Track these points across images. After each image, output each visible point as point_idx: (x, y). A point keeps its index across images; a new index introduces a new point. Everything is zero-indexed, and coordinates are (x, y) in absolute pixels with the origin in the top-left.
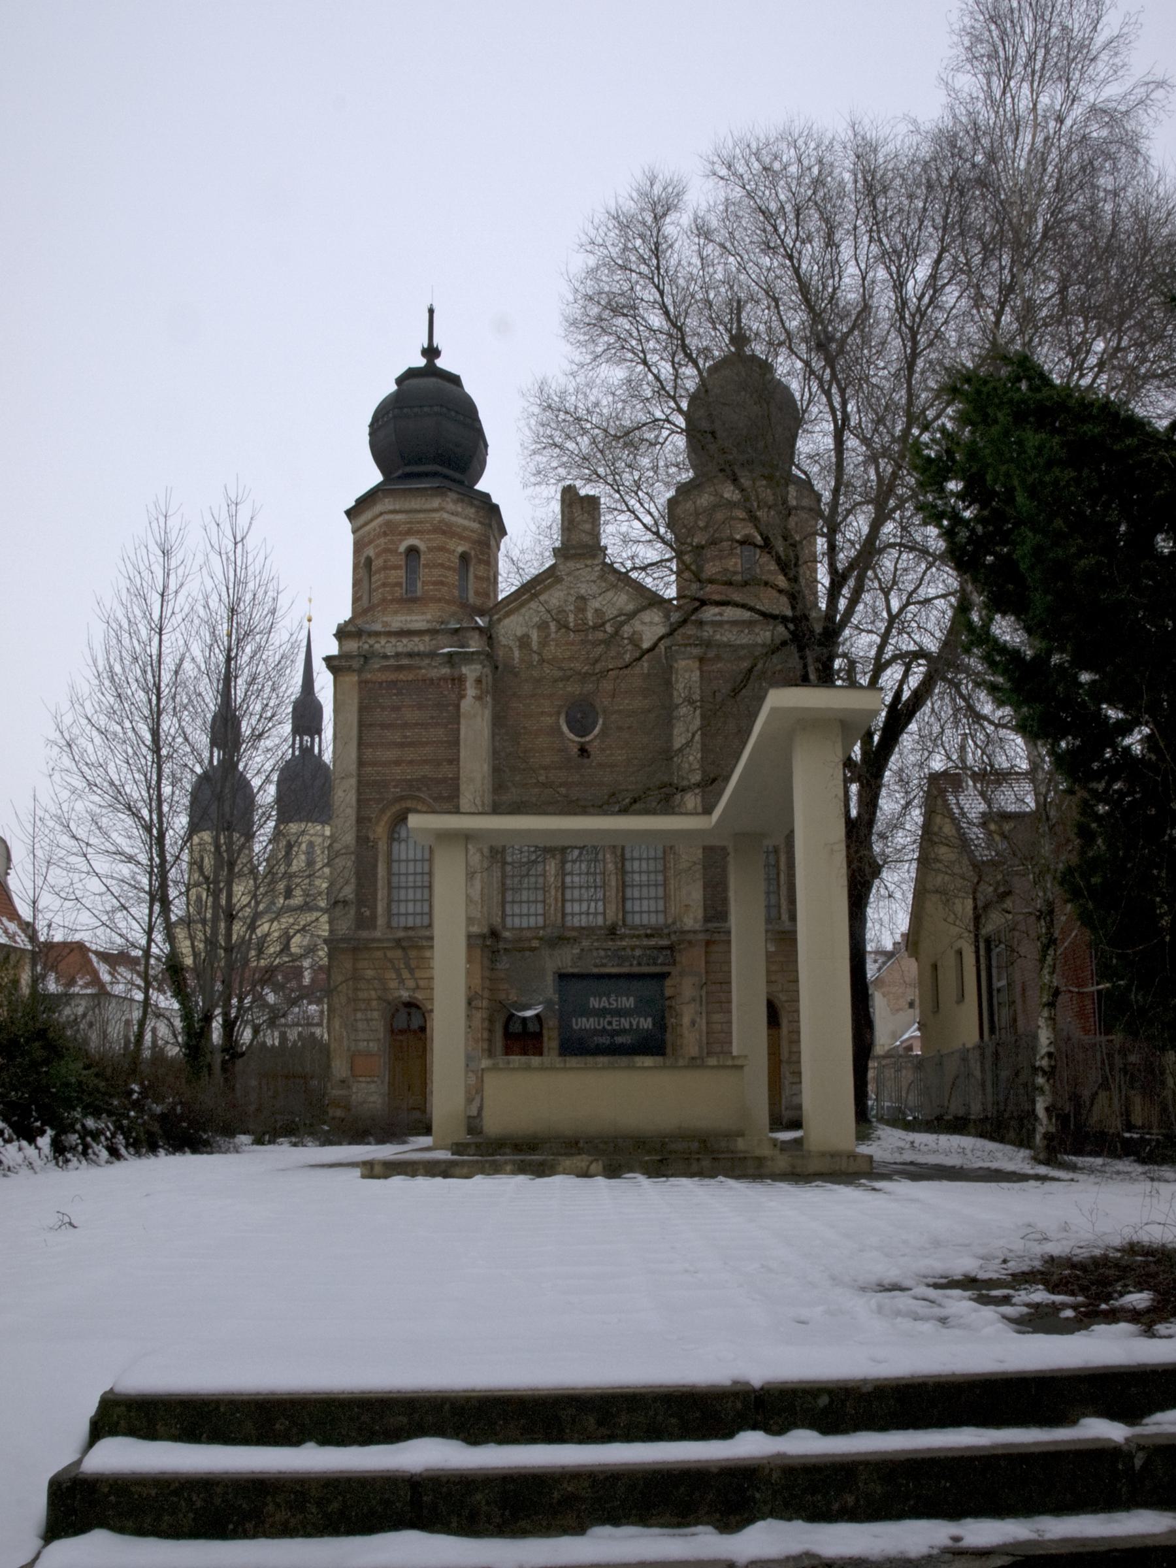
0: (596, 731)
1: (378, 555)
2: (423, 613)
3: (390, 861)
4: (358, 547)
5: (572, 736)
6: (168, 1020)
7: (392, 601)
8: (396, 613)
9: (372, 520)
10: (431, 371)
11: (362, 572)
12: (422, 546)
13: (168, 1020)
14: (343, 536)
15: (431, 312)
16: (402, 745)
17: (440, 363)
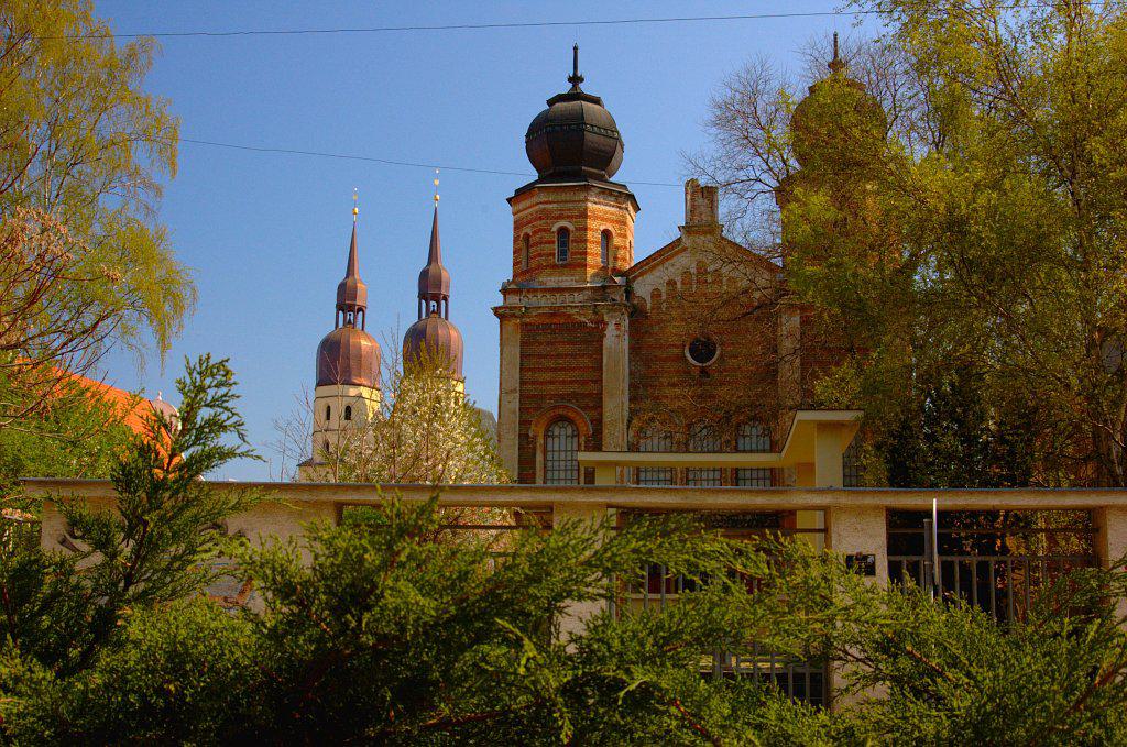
0: (714, 360)
1: (535, 233)
2: (572, 275)
3: (545, 452)
4: (518, 226)
5: (694, 362)
6: (142, 356)
7: (547, 267)
8: (550, 275)
9: (530, 207)
10: (575, 95)
11: (521, 244)
12: (571, 227)
13: (142, 356)
14: (506, 217)
15: (575, 49)
16: (555, 370)
17: (585, 88)
